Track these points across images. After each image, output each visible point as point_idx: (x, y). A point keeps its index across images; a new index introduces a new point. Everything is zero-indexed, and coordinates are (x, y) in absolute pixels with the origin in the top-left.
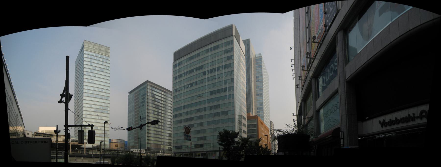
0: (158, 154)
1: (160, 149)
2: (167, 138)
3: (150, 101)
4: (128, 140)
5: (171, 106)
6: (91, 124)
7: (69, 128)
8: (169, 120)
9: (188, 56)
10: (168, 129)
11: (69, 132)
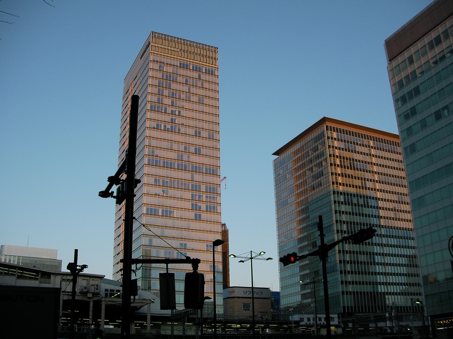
0: (380, 324)
1: (385, 308)
2: (403, 270)
3: (338, 162)
4: (282, 288)
5: (403, 174)
6: (193, 256)
7: (133, 267)
8: (396, 165)
9: (426, 40)
10: (402, 242)
11: (133, 277)
